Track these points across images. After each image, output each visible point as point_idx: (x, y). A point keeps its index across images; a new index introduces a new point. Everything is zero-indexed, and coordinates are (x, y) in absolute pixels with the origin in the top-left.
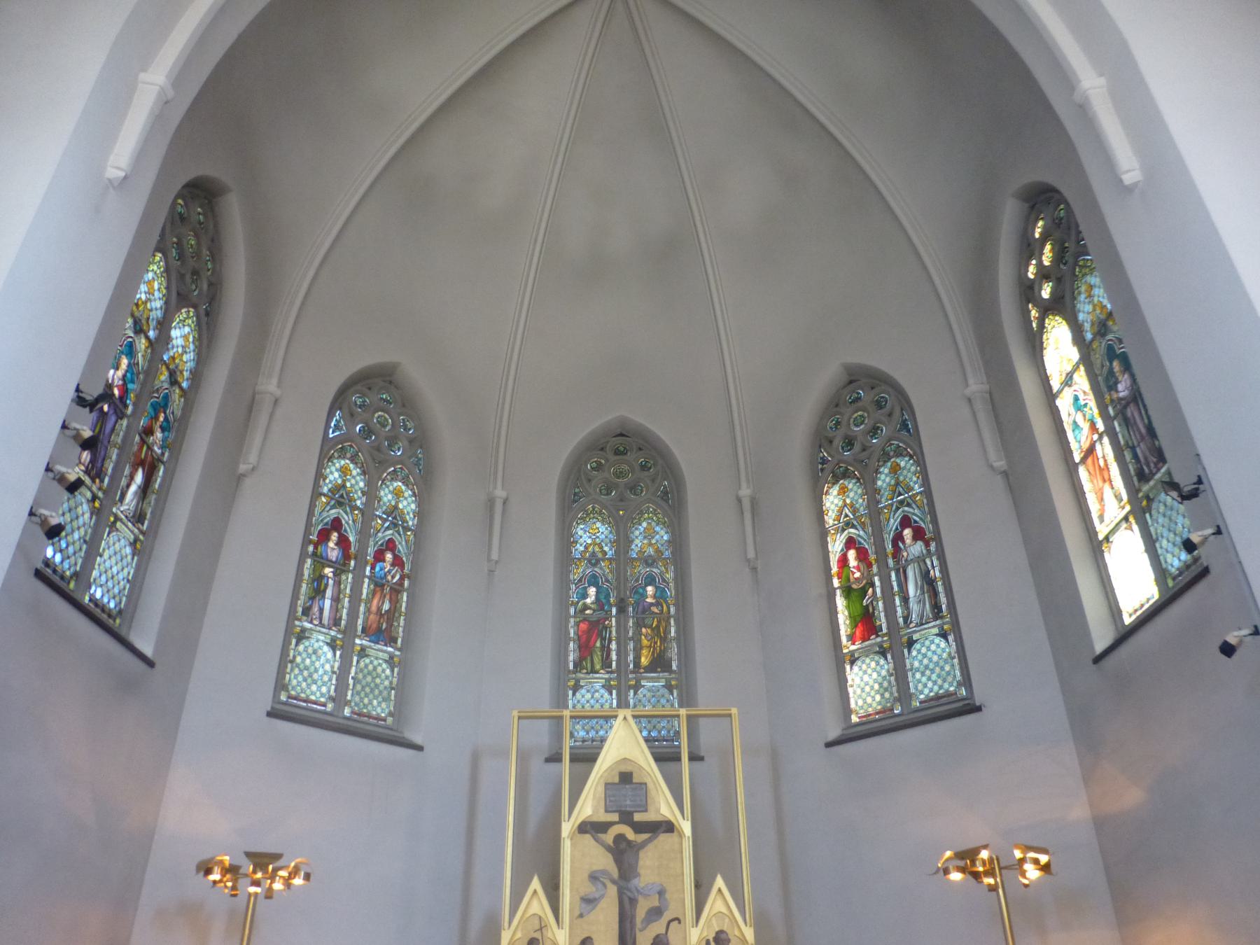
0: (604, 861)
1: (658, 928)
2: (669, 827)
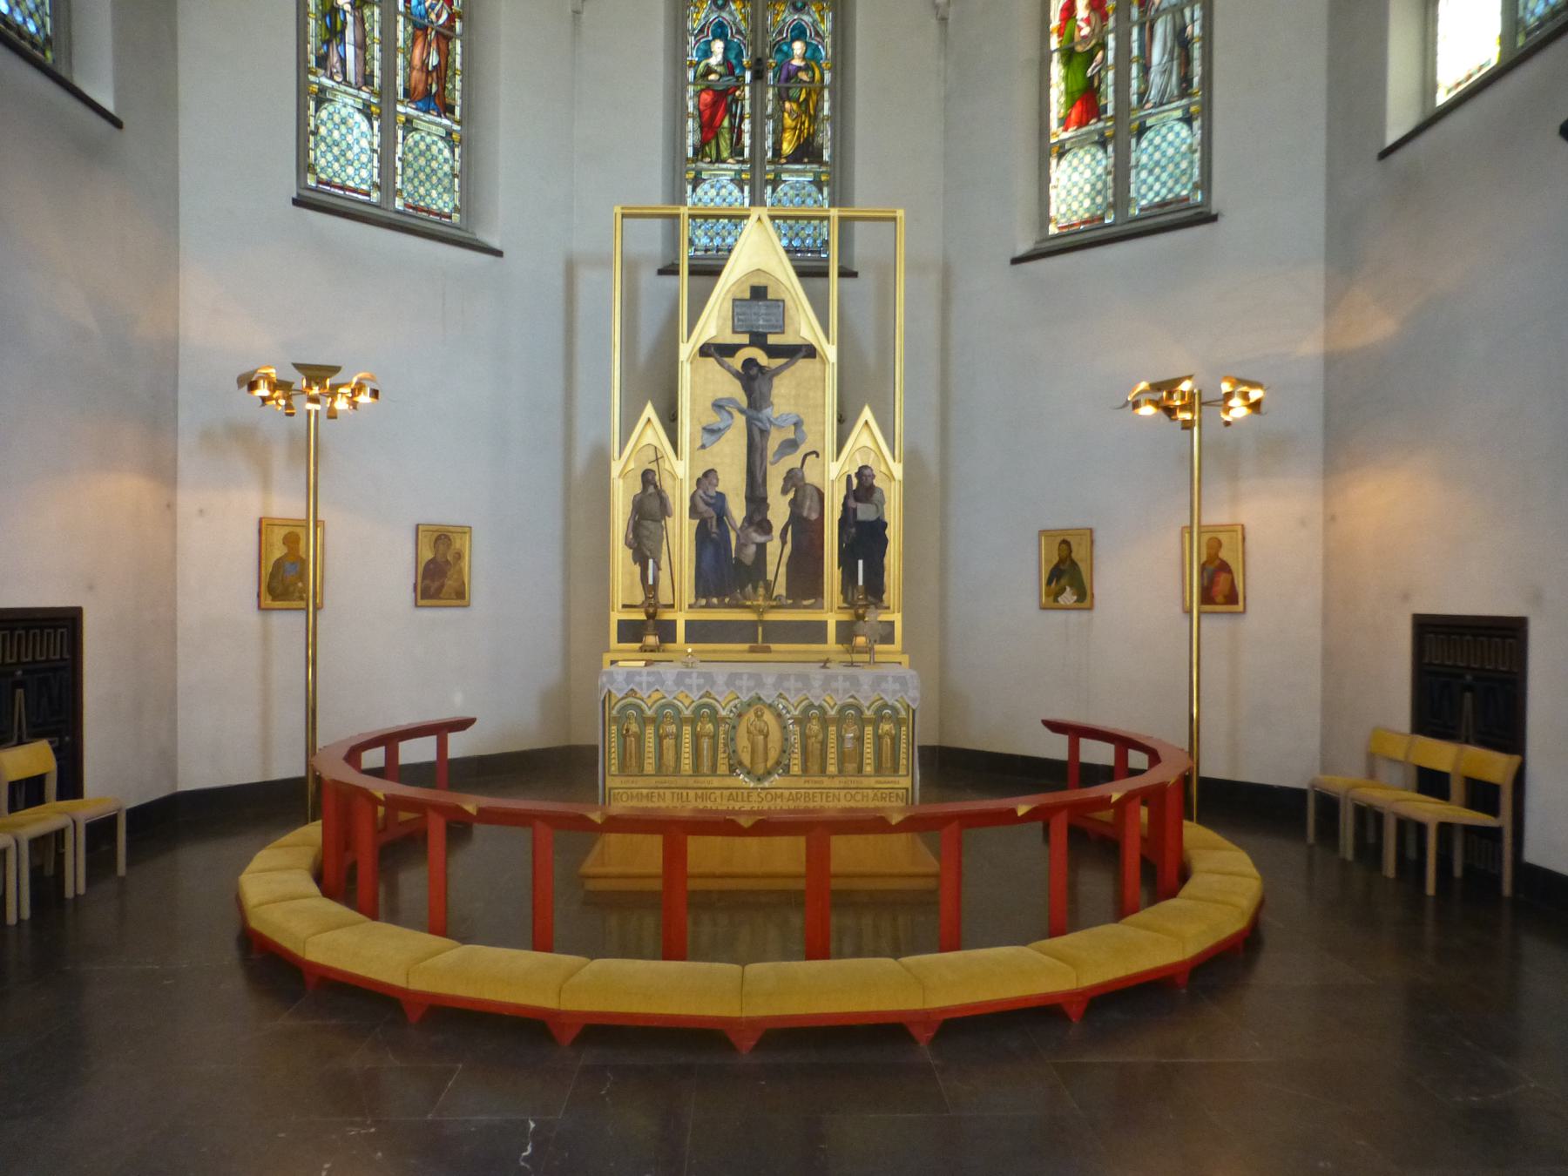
1: (793, 461)
2: (810, 352)
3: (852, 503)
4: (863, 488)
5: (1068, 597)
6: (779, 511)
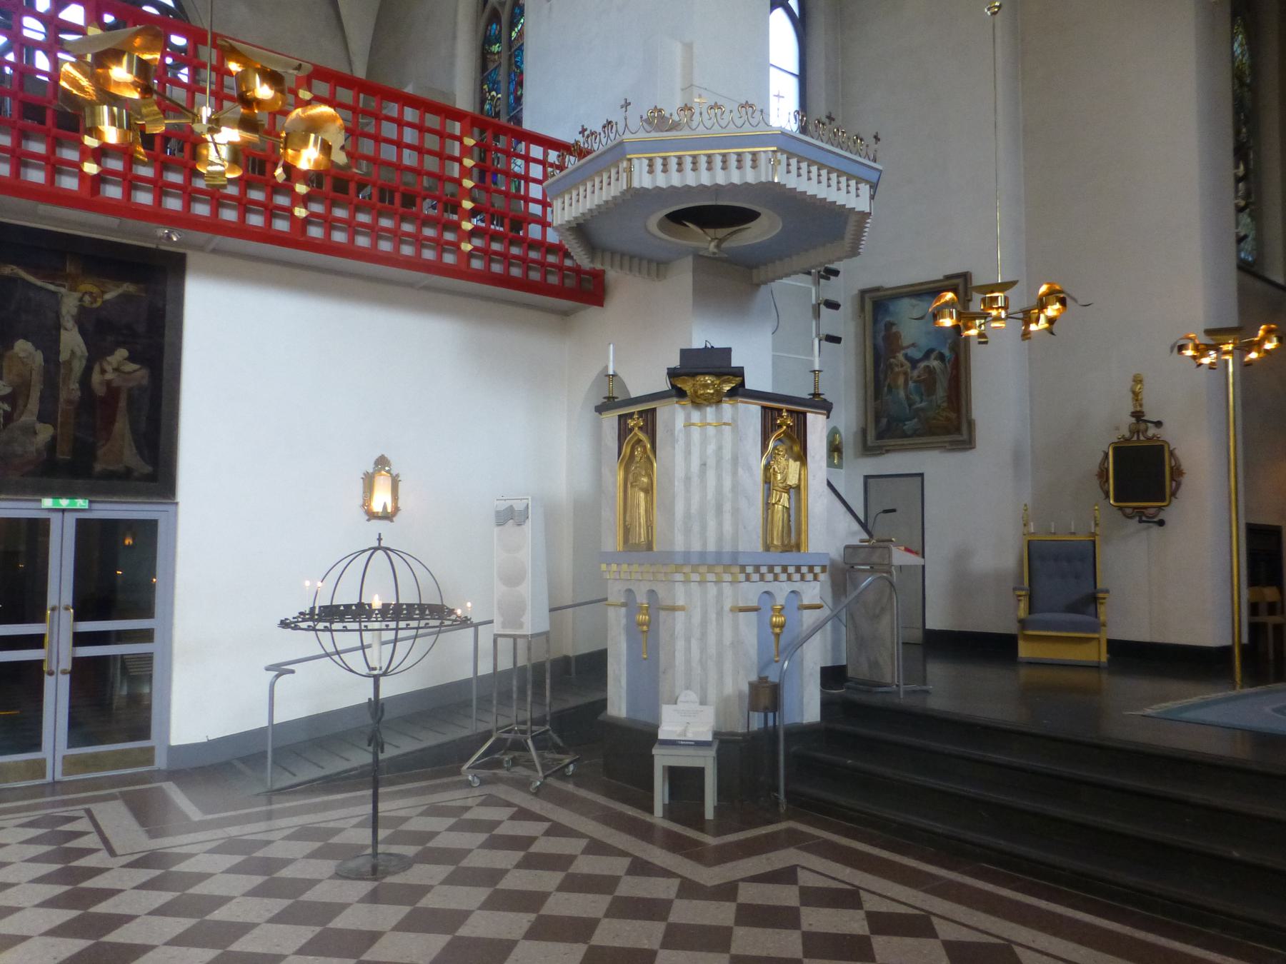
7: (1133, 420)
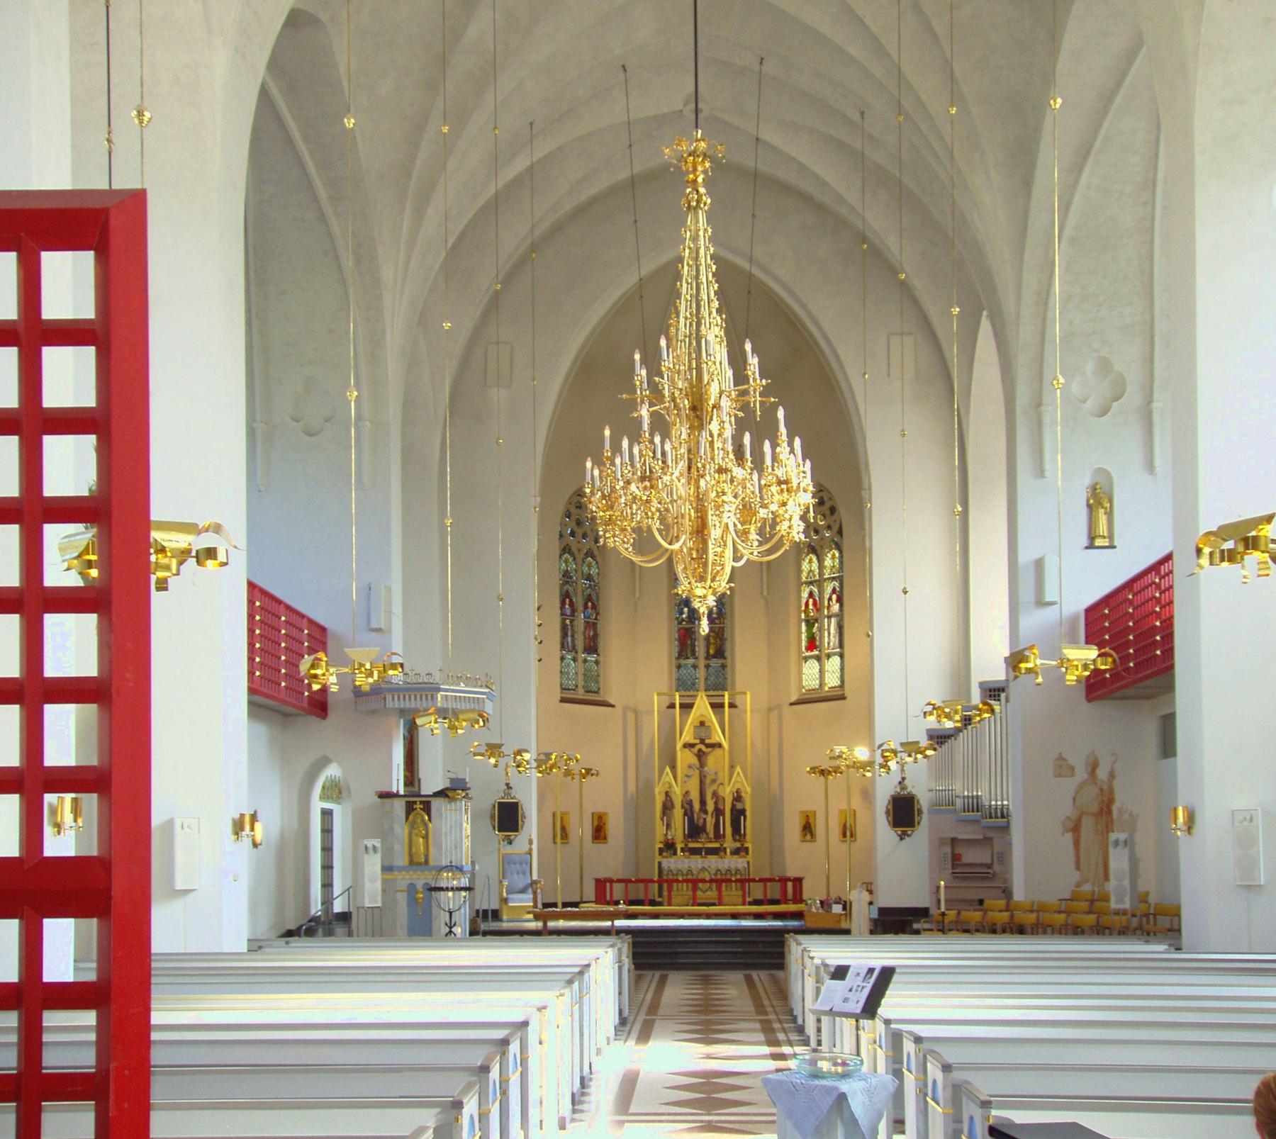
0: (694, 760)
1: (714, 787)
2: (720, 745)
3: (735, 803)
4: (738, 798)
5: (808, 837)
6: (710, 807)
7: (506, 787)
